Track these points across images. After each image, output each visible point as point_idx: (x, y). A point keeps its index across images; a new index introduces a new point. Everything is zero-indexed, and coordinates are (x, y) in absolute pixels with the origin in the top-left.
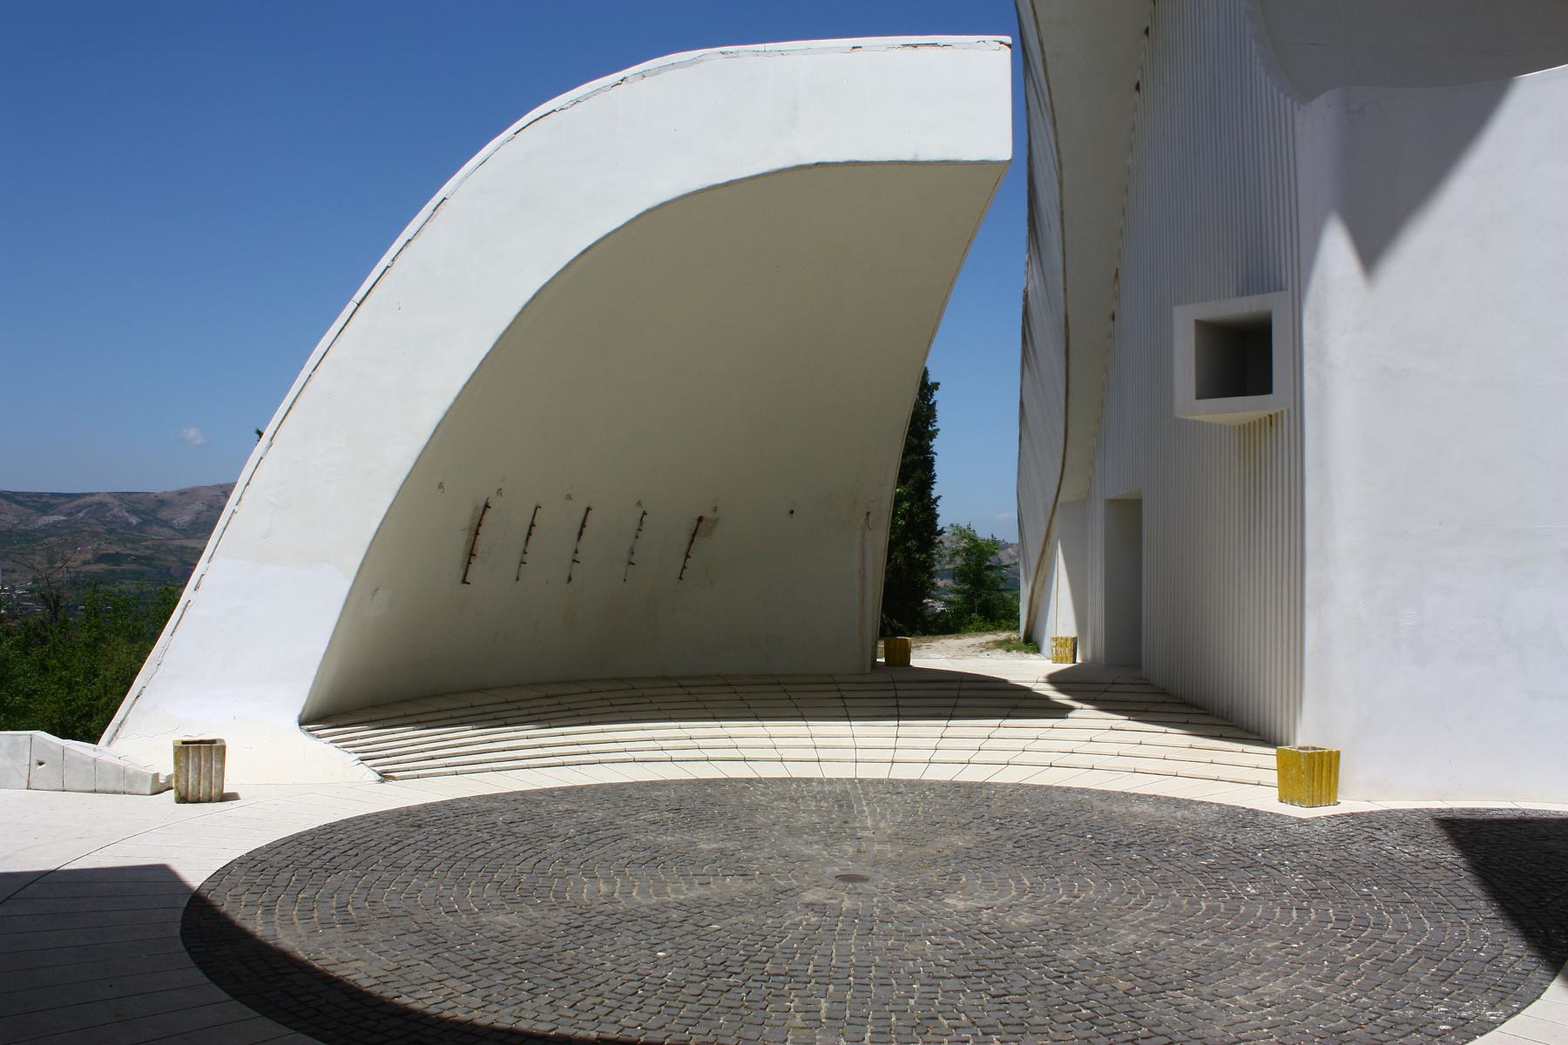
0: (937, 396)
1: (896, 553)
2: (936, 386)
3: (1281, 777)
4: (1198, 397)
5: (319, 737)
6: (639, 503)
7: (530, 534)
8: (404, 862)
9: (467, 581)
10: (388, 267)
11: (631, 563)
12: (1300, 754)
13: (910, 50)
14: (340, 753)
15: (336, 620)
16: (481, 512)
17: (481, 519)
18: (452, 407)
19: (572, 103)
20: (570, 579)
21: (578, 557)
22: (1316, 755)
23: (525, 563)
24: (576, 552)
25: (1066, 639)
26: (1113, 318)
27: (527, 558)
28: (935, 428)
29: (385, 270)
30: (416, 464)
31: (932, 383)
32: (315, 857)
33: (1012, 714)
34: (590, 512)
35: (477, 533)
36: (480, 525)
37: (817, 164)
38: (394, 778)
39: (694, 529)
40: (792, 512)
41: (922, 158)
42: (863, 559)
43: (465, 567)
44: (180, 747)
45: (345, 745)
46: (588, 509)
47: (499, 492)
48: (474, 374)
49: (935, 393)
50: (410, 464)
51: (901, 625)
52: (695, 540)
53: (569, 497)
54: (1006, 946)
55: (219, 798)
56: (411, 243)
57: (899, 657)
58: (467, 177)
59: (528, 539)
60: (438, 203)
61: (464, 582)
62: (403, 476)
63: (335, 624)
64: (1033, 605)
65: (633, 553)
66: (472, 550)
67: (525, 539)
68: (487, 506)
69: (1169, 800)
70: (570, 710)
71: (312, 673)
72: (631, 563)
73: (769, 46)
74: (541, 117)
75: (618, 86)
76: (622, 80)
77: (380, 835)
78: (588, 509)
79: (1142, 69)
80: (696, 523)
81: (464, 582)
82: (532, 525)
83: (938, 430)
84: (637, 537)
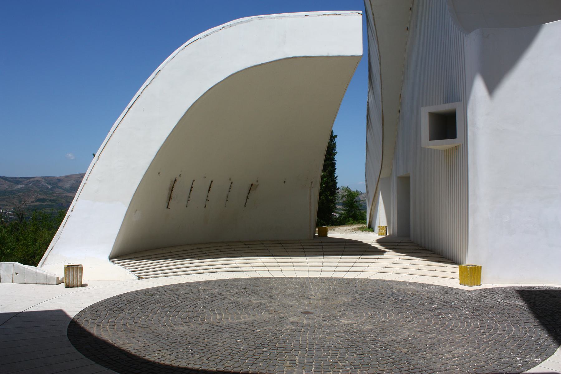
2: (336, 136)
3: (461, 276)
4: (430, 140)
5: (116, 263)
6: (230, 179)
7: (191, 190)
9: (169, 207)
10: (139, 95)
13: (326, 16)
14: (124, 269)
16: (173, 183)
17: (173, 185)
20: (205, 206)
21: (208, 199)
24: (208, 197)
25: (383, 227)
29: (138, 96)
30: (150, 166)
31: (335, 135)
36: (173, 187)
37: (293, 57)
39: (250, 188)
40: (285, 182)
41: (331, 55)
45: (125, 266)
46: (212, 181)
47: (180, 175)
48: (170, 134)
49: (336, 139)
50: (148, 166)
51: (324, 222)
57: (324, 234)
58: (168, 62)
60: (157, 72)
61: (168, 208)
66: (170, 196)
68: (175, 181)
73: (272, 15)
76: (223, 28)
77: (138, 298)
78: (212, 181)
79: (409, 22)
80: (251, 186)
81: (168, 208)
82: (192, 187)
83: (337, 152)
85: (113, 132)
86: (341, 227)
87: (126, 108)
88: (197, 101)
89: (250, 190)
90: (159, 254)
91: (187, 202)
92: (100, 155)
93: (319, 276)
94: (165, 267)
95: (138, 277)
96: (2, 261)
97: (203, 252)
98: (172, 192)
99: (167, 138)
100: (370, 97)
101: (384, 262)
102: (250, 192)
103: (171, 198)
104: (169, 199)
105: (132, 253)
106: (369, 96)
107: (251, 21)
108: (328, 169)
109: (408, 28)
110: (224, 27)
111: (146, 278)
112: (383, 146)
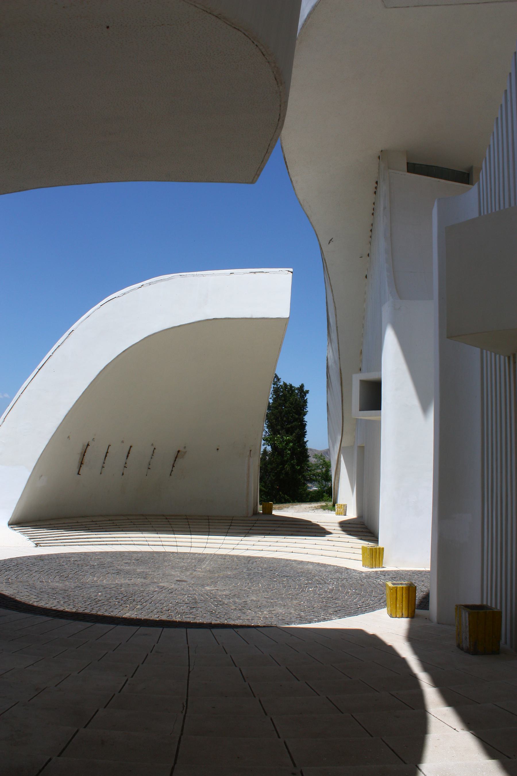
0: (308, 396)
1: (286, 466)
2: (307, 392)
3: (363, 557)
4: (360, 410)
5: (15, 530)
6: (152, 445)
7: (106, 456)
8: (32, 569)
9: (80, 473)
10: (51, 356)
11: (149, 468)
12: (367, 548)
13: (253, 274)
14: (22, 536)
15: (24, 487)
16: (86, 447)
17: (86, 450)
18: (71, 409)
19: (123, 294)
20: (123, 474)
21: (126, 465)
22: (374, 549)
23: (104, 467)
24: (126, 463)
25: (342, 505)
26: (360, 370)
27: (104, 465)
28: (306, 410)
29: (50, 357)
30: (57, 430)
31: (306, 391)
33: (316, 535)
34: (131, 448)
35: (84, 455)
36: (85, 452)
37: (214, 319)
38: (40, 546)
39: (176, 455)
40: (218, 449)
41: (254, 317)
42: (249, 469)
43: (79, 468)
45: (24, 533)
46: (131, 447)
47: (93, 439)
48: (80, 397)
49: (307, 395)
50: (55, 429)
51: (288, 498)
52: (176, 460)
53: (123, 442)
56: (60, 347)
57: (268, 511)
58: (82, 322)
59: (105, 458)
60: (70, 332)
62: (52, 434)
63: (24, 489)
64: (335, 490)
66: (82, 462)
67: (104, 458)
68: (88, 445)
69: (318, 564)
70: (116, 525)
71: (14, 506)
72: (149, 468)
73: (195, 273)
74: (111, 300)
75: (140, 288)
76: (142, 286)
77: (28, 562)
78: (131, 447)
79: (367, 269)
81: (78, 474)
82: (107, 452)
83: (307, 411)
85: (21, 394)
86: (304, 504)
87: (36, 368)
88: (108, 364)
89: (176, 458)
90: (64, 523)
91: (102, 468)
92: (6, 416)
94: (67, 536)
95: (36, 544)
97: (114, 524)
98: (84, 457)
99: (77, 401)
100: (329, 352)
101: (307, 543)
103: (83, 464)
104: (80, 464)
105: (34, 521)
106: (328, 350)
107: (173, 278)
108: (295, 432)
109: (366, 275)
110: (143, 285)
111: (44, 546)
112: (342, 409)
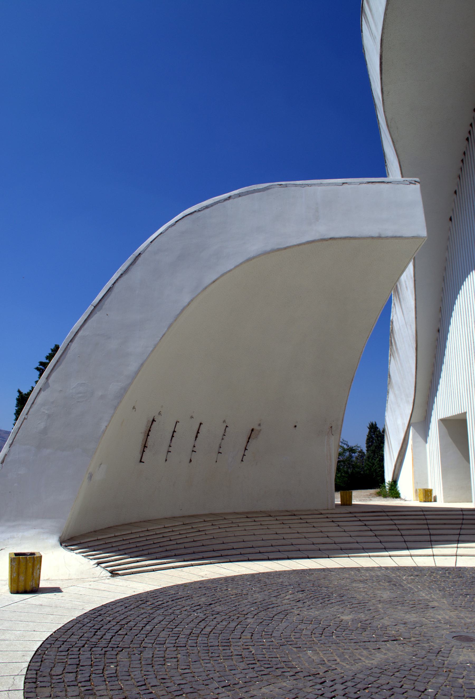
7: (173, 436)
9: (142, 461)
13: (370, 185)
14: (86, 560)
16: (150, 424)
17: (150, 427)
20: (191, 461)
24: (194, 447)
32: (99, 637)
34: (202, 425)
35: (148, 435)
36: (150, 431)
38: (118, 574)
39: (249, 435)
40: (295, 426)
44: (14, 558)
46: (201, 424)
47: (160, 413)
54: (392, 658)
55: (15, 592)
57: (347, 502)
61: (141, 461)
65: (220, 447)
66: (145, 444)
68: (154, 420)
72: (219, 453)
78: (201, 424)
80: (251, 432)
81: (141, 461)
82: (174, 431)
84: (223, 439)
89: (249, 438)
93: (453, 565)
96: (52, 653)
102: (250, 440)
